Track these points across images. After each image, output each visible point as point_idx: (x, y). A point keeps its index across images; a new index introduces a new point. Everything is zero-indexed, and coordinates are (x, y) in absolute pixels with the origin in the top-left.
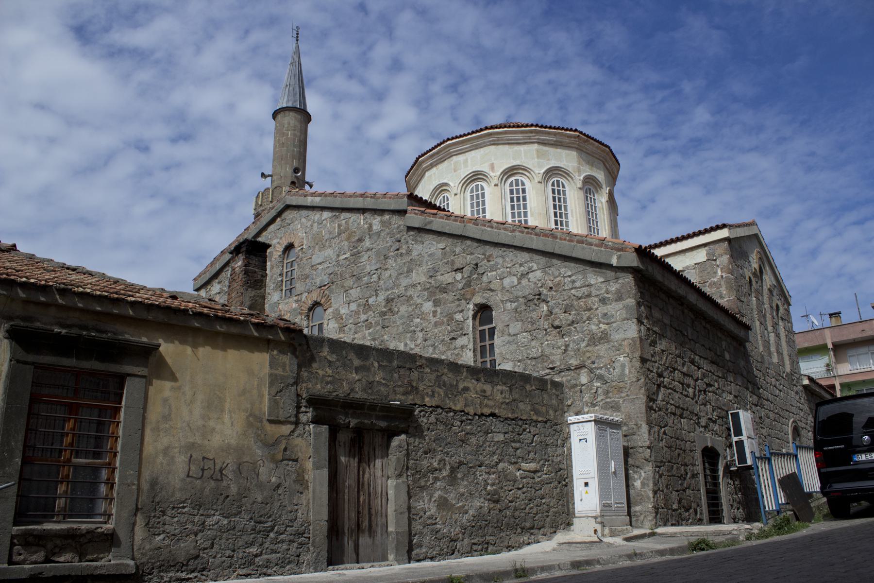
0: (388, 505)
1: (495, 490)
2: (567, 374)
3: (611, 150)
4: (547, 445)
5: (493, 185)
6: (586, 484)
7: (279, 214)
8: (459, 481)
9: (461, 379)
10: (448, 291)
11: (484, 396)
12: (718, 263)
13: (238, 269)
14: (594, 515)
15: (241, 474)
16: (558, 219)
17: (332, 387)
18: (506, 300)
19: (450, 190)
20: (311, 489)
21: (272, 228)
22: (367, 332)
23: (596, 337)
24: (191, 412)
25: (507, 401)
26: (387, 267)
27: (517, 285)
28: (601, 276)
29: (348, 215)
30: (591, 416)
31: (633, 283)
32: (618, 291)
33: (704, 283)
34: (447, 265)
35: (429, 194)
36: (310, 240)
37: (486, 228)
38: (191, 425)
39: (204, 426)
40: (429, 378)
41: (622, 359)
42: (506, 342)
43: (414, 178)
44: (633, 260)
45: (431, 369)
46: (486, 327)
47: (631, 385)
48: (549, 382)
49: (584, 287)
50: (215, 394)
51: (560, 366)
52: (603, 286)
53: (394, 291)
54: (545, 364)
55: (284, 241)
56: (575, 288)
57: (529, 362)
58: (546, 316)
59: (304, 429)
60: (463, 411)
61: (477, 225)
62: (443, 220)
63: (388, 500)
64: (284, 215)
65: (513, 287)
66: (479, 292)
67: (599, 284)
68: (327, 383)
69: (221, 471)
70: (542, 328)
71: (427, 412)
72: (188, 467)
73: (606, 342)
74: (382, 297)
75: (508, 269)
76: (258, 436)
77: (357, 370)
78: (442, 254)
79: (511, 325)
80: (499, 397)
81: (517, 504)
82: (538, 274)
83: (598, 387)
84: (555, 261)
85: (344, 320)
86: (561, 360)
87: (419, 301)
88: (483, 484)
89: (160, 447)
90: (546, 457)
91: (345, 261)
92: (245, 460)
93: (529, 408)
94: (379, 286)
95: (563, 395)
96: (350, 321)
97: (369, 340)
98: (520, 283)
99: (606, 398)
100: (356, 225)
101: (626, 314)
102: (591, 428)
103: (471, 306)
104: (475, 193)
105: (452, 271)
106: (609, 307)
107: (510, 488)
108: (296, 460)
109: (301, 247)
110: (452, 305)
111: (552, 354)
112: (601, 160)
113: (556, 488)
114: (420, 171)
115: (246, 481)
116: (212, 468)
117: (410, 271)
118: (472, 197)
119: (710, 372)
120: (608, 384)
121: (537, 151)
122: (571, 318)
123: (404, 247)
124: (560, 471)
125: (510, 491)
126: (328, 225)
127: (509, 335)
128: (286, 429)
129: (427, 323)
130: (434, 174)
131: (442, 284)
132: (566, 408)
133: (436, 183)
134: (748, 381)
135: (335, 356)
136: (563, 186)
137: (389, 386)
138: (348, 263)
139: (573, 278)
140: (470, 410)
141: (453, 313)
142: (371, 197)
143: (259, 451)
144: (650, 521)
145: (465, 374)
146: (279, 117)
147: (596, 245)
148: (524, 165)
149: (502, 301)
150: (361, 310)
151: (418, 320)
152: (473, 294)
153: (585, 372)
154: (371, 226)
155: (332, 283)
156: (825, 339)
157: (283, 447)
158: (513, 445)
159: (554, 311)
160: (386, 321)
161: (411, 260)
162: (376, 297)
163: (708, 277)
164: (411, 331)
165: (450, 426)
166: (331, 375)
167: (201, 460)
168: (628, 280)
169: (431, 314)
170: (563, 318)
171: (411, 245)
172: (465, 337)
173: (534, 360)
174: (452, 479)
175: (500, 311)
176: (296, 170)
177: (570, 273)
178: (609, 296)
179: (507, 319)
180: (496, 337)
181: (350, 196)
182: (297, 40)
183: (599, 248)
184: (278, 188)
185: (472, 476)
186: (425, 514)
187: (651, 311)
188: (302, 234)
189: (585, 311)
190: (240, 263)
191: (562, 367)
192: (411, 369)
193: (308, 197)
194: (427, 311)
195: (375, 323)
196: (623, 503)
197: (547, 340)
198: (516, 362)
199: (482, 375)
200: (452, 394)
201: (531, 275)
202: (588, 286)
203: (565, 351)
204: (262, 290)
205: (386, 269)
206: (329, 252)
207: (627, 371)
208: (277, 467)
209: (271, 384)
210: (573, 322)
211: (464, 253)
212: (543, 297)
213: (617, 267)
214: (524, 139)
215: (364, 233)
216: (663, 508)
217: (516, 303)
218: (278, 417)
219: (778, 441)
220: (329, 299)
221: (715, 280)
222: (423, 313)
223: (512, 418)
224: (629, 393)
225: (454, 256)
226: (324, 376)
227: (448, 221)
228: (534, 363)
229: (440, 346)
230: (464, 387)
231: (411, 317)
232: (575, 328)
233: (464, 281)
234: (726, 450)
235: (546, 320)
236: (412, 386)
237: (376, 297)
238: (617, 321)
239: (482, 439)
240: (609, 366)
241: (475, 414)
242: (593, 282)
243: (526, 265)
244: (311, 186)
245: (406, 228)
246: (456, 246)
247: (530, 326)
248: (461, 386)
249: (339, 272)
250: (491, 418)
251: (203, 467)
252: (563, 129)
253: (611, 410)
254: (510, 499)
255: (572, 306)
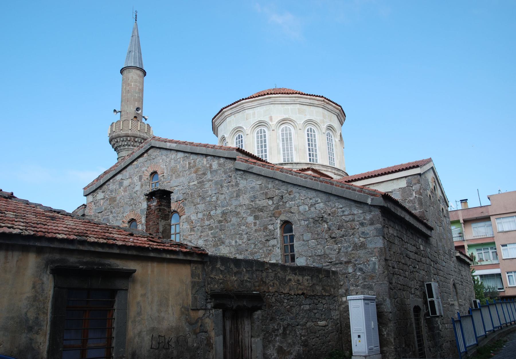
0: (252, 354)
1: (306, 339)
2: (340, 266)
3: (342, 108)
4: (330, 310)
5: (271, 130)
6: (359, 336)
7: (147, 151)
8: (288, 335)
9: (287, 274)
10: (263, 211)
11: (299, 283)
12: (413, 188)
13: (153, 207)
14: (364, 355)
15: (178, 343)
16: (311, 152)
17: (223, 286)
18: (302, 220)
19: (243, 131)
20: (214, 349)
21: (141, 160)
22: (210, 232)
23: (357, 246)
24: (152, 309)
25: (310, 285)
26: (222, 192)
27: (308, 211)
28: (361, 210)
29: (195, 157)
30: (362, 296)
31: (380, 215)
32: (371, 219)
33: (405, 200)
34: (263, 195)
35: (230, 133)
36: (169, 170)
37: (288, 175)
38: (152, 317)
39: (159, 316)
40: (271, 275)
41: (374, 260)
42: (301, 244)
43: (218, 121)
44: (381, 202)
45: (272, 270)
46: (288, 234)
47: (380, 275)
48: (331, 272)
49: (350, 215)
50: (164, 296)
51: (335, 261)
52: (362, 215)
53: (227, 208)
54: (326, 259)
55: (150, 170)
56: (345, 215)
57: (316, 257)
58: (326, 231)
59: (209, 312)
60: (289, 294)
61: (283, 172)
62: (261, 167)
63: (252, 350)
64: (149, 152)
65: (306, 212)
66: (283, 213)
67: (359, 214)
68: (221, 283)
69: (169, 342)
70: (324, 238)
71: (270, 296)
72: (151, 343)
73: (364, 249)
74: (219, 211)
75: (302, 201)
76: (187, 319)
77: (236, 274)
78: (259, 187)
79: (305, 235)
80: (306, 283)
81: (317, 346)
82: (322, 205)
83: (359, 275)
84: (332, 198)
85: (194, 223)
86: (336, 258)
87: (245, 215)
88: (299, 336)
89: (136, 332)
90: (330, 317)
91: (193, 186)
92: (180, 335)
93: (321, 288)
94: (217, 204)
95: (338, 279)
96: (198, 225)
97: (211, 237)
98: (310, 209)
99: (364, 282)
100: (201, 164)
101: (376, 233)
102: (361, 303)
103: (279, 221)
104: (259, 134)
105: (266, 199)
106: (366, 228)
107: (313, 337)
108: (206, 332)
109: (163, 174)
110: (266, 220)
111: (330, 254)
112: (336, 115)
113: (336, 335)
114: (223, 117)
115: (181, 347)
116: (164, 342)
117: (238, 196)
118: (258, 137)
119: (415, 259)
120: (365, 274)
121: (299, 109)
122: (342, 233)
123: (233, 181)
124: (337, 324)
125: (313, 339)
126: (182, 162)
127: (304, 240)
128: (201, 313)
129: (250, 230)
130: (233, 120)
131: (260, 206)
132: (340, 286)
133: (234, 126)
134: (431, 261)
135: (224, 267)
136: (314, 132)
137: (251, 282)
138: (196, 188)
139: (343, 209)
140: (292, 293)
141: (267, 225)
142: (212, 148)
143: (188, 329)
144: (393, 356)
145: (289, 271)
146: (125, 72)
147: (358, 191)
148: (291, 118)
149: (299, 220)
150: (206, 218)
151: (244, 227)
152: (280, 214)
153: (351, 266)
154: (211, 166)
155: (185, 199)
156: (458, 217)
157: (200, 324)
158: (314, 311)
159: (332, 228)
160: (223, 226)
161: (239, 189)
162: (216, 211)
163: (407, 197)
164: (240, 234)
165: (282, 303)
166: (222, 278)
167: (158, 337)
168: (377, 213)
169: (253, 224)
170: (338, 233)
171: (239, 180)
172: (275, 240)
173: (319, 257)
174: (284, 334)
175: (297, 226)
176: (138, 109)
177: (341, 206)
178: (366, 222)
179: (302, 231)
180: (295, 241)
181: (197, 146)
182: (136, 20)
183: (360, 193)
184: (126, 121)
185: (294, 332)
186: (271, 357)
187: (388, 230)
188: (163, 166)
189: (351, 229)
190: (155, 204)
191: (337, 262)
192: (262, 271)
193: (167, 143)
194: (250, 222)
195: (215, 227)
196: (378, 346)
197: (327, 245)
198: (308, 257)
199: (297, 271)
200: (283, 284)
201: (317, 205)
202: (352, 215)
203: (339, 252)
204: (169, 220)
205: (222, 194)
206: (182, 179)
207: (377, 267)
208: (197, 337)
209: (193, 287)
210: (343, 236)
211: (274, 188)
212: (324, 219)
213: (371, 205)
214: (291, 101)
215: (207, 169)
216: (399, 348)
217: (307, 222)
218: (196, 307)
219: (446, 294)
220: (183, 209)
221: (412, 199)
222: (247, 223)
223: (313, 295)
224: (378, 280)
225: (268, 189)
226: (219, 279)
227: (264, 168)
228: (319, 259)
229: (259, 244)
230: (289, 279)
231: (239, 225)
232: (345, 239)
233: (274, 206)
234: (423, 306)
235: (327, 233)
236: (263, 281)
237: (216, 211)
238: (371, 237)
239: (298, 309)
240: (366, 263)
241: (295, 295)
242: (355, 212)
243: (314, 199)
244: (146, 120)
245: (235, 169)
246: (268, 184)
247: (316, 236)
248: (287, 279)
249: (190, 193)
250: (302, 296)
251: (159, 341)
252: (315, 95)
253: (367, 289)
254: (313, 344)
255: (343, 226)
